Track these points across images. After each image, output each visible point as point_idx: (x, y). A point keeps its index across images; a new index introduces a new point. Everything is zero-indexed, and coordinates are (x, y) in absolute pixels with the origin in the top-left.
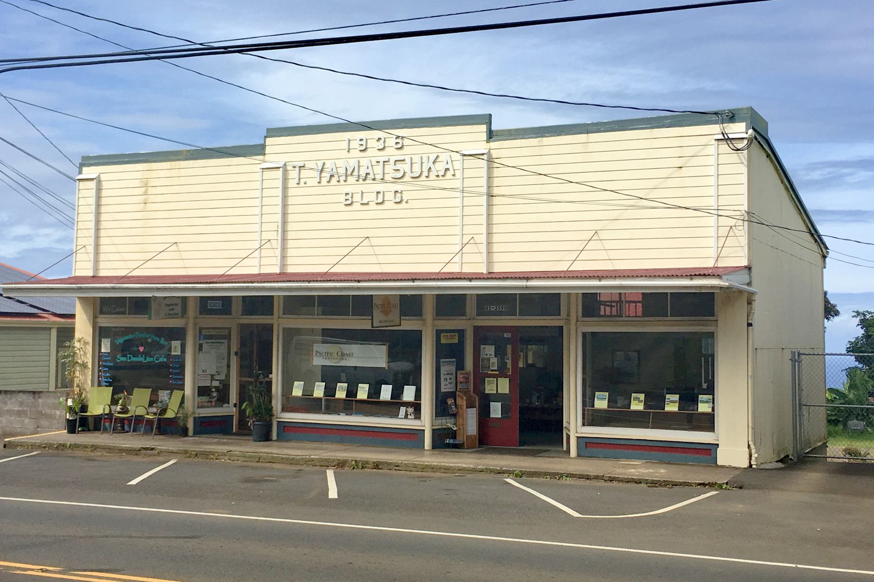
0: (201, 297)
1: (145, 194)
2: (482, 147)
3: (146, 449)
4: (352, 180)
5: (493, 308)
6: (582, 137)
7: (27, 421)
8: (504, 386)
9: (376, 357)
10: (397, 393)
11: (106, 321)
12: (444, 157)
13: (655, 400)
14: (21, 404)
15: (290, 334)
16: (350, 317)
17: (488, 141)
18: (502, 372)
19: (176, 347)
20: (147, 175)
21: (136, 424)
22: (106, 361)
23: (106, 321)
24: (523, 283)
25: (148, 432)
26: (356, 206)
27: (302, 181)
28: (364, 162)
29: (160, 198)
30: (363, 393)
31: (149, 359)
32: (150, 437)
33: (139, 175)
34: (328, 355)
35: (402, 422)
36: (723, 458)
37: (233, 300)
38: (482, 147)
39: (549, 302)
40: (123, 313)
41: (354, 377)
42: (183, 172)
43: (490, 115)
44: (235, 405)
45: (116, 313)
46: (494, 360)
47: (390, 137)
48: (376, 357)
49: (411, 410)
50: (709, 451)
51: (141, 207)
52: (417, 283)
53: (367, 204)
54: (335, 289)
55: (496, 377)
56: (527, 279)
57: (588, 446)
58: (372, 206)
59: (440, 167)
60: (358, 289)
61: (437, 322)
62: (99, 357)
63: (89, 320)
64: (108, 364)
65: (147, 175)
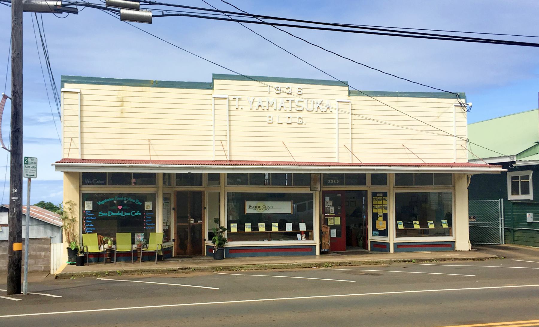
0: (209, 174)
1: (122, 106)
2: (346, 98)
3: (180, 269)
4: (271, 109)
5: (332, 182)
6: (395, 99)
8: (337, 221)
9: (285, 208)
10: (296, 227)
11: (89, 189)
12: (257, 99)
13: (423, 224)
15: (374, 194)
16: (345, 186)
17: (349, 96)
18: (336, 214)
20: (122, 93)
21: (126, 257)
22: (89, 216)
23: (89, 189)
24: (417, 168)
26: (275, 124)
27: (240, 107)
28: (280, 100)
30: (275, 228)
33: (116, 93)
34: (256, 208)
35: (301, 242)
36: (458, 247)
38: (346, 98)
39: (148, 178)
40: (104, 184)
41: (268, 220)
42: (152, 95)
43: (213, 74)
44: (174, 240)
45: (96, 184)
46: (332, 208)
47: (295, 87)
48: (285, 208)
49: (304, 236)
50: (450, 246)
51: (119, 114)
52: (331, 167)
55: (333, 216)
56: (418, 166)
57: (399, 247)
58: (285, 125)
59: (256, 104)
60: (329, 170)
62: (84, 214)
63: (76, 189)
65: (122, 93)
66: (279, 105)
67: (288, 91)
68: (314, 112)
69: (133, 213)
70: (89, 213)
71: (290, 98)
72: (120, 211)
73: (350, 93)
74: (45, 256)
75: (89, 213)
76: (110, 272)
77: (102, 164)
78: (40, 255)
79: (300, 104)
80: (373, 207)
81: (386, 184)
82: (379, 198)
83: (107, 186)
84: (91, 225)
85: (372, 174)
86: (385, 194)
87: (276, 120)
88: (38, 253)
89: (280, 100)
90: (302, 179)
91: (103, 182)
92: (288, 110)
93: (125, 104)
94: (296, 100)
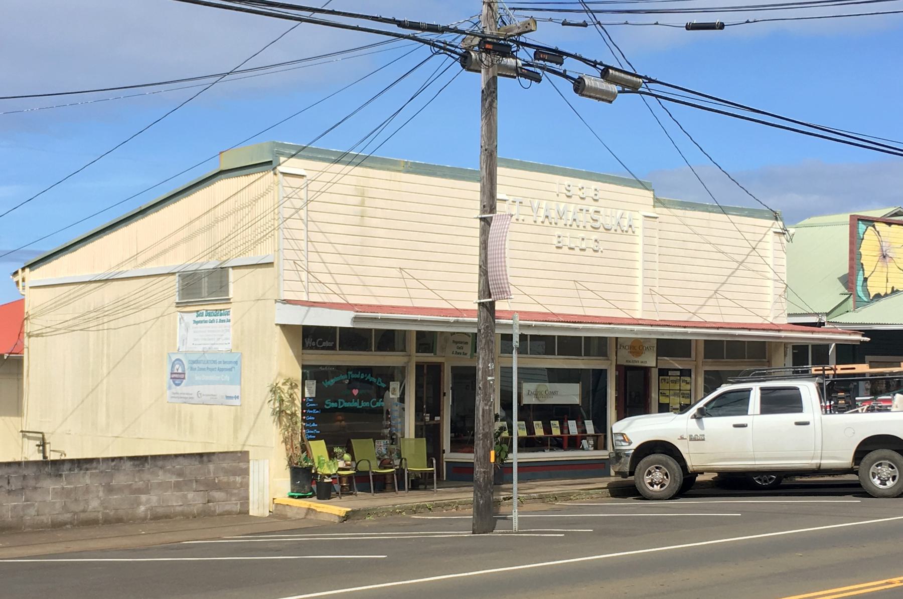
1: (362, 204)
4: (561, 223)
7: (190, 495)
9: (569, 394)
14: (180, 474)
15: (663, 372)
19: (394, 389)
25: (347, 491)
26: (565, 250)
29: (379, 213)
31: (365, 404)
32: (369, 495)
33: (353, 180)
37: (396, 333)
39: (388, 340)
40: (333, 348)
45: (323, 348)
49: (592, 442)
51: (357, 220)
53: (573, 249)
54: (676, 333)
58: (589, 252)
61: (306, 357)
64: (314, 411)
66: (570, 216)
67: (580, 193)
68: (613, 231)
69: (374, 404)
70: (311, 403)
71: (583, 205)
72: (356, 398)
73: (658, 202)
74: (241, 483)
75: (311, 403)
76: (418, 507)
77: (419, 317)
78: (234, 482)
79: (596, 216)
80: (661, 393)
81: (690, 357)
82: (672, 378)
83: (338, 352)
84: (314, 425)
85: (705, 341)
86: (686, 373)
87: (567, 242)
88: (232, 479)
89: (572, 207)
90: (597, 346)
91: (331, 344)
92: (581, 227)
93: (368, 202)
94: (592, 209)
